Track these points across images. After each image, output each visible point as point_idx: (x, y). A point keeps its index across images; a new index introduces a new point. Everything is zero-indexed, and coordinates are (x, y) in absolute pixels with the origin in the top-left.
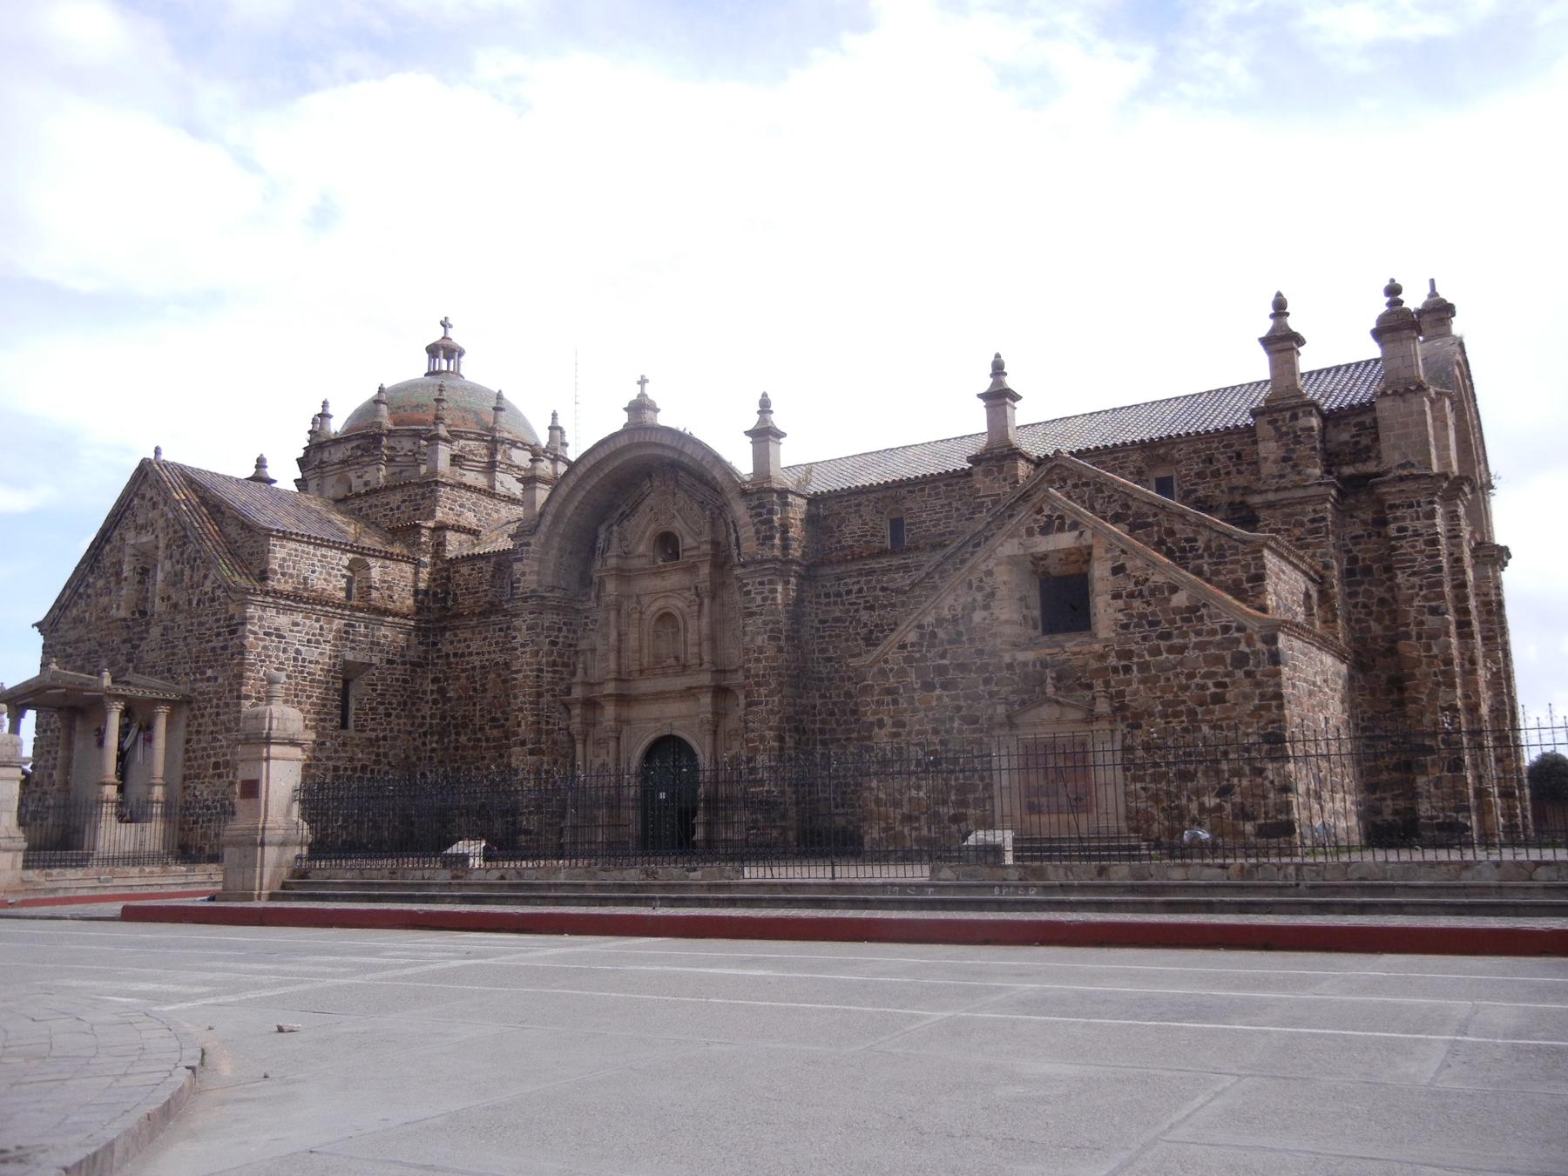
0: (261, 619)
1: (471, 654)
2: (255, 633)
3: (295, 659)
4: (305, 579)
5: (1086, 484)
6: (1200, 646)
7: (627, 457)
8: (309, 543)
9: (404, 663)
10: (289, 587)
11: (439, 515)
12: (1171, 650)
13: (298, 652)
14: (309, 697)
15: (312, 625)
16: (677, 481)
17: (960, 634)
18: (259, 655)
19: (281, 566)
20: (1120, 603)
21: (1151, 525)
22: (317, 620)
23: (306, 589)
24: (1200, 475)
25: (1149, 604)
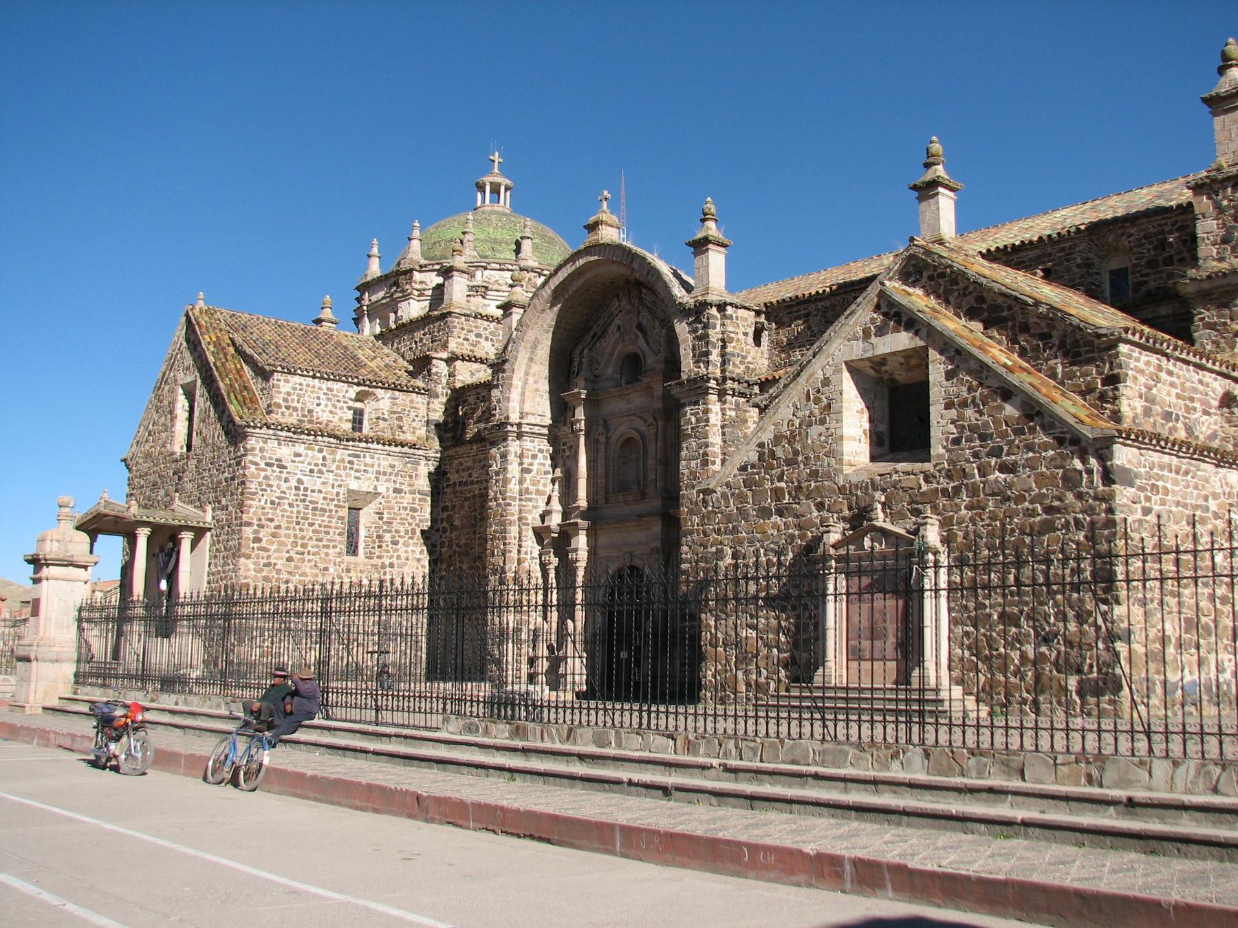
0: (262, 450)
1: (472, 483)
2: (256, 464)
3: (297, 488)
4: (310, 411)
5: (942, 275)
6: (1031, 465)
7: (589, 275)
8: (314, 377)
9: (413, 492)
10: (292, 419)
11: (453, 345)
12: (1003, 468)
13: (300, 481)
14: (311, 525)
15: (314, 456)
16: (641, 299)
17: (796, 453)
18: (260, 484)
19: (285, 400)
20: (953, 413)
21: (1005, 320)
22: (321, 451)
23: (310, 422)
24: (1151, 264)
25: (981, 414)
